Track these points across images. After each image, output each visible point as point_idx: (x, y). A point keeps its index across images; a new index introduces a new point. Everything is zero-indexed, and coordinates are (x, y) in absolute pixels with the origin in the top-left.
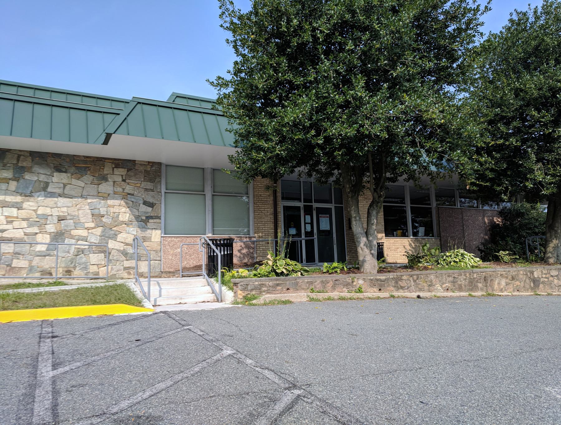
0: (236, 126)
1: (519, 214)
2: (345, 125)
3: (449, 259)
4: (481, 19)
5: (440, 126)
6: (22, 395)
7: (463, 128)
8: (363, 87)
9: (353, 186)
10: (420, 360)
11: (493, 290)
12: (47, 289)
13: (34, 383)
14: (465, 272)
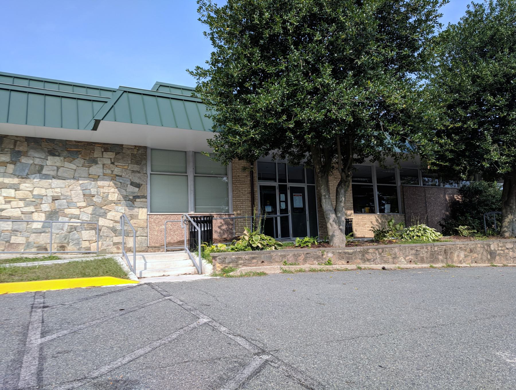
0: (214, 112)
1: (477, 192)
2: (313, 111)
3: (412, 234)
4: (440, 10)
5: (402, 111)
6: (11, 361)
7: (423, 112)
8: (330, 75)
9: (322, 166)
10: (382, 327)
11: (453, 262)
12: (41, 263)
13: (23, 349)
14: (427, 245)
